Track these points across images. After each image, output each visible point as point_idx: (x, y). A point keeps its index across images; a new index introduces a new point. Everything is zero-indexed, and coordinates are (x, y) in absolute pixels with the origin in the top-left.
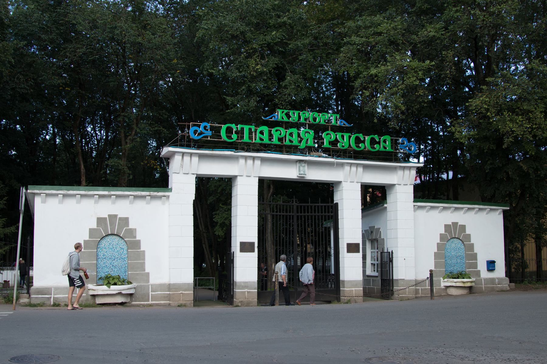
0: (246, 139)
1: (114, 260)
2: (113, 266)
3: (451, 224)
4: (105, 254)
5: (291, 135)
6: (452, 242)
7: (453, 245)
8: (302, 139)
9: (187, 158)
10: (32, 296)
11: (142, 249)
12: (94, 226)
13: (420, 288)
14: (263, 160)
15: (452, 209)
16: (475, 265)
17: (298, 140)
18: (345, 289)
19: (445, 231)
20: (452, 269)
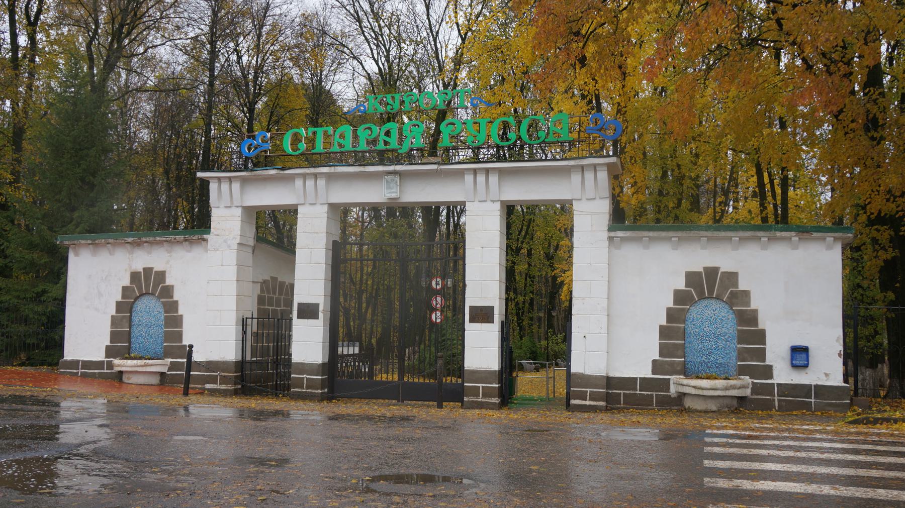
0: (319, 147)
1: (150, 327)
2: (148, 335)
4: (141, 319)
5: (388, 133)
6: (707, 306)
7: (708, 312)
9: (310, 183)
12: (681, 285)
13: (654, 394)
14: (501, 171)
16: (761, 354)
17: (499, 134)
19: (131, 283)
20: (703, 359)
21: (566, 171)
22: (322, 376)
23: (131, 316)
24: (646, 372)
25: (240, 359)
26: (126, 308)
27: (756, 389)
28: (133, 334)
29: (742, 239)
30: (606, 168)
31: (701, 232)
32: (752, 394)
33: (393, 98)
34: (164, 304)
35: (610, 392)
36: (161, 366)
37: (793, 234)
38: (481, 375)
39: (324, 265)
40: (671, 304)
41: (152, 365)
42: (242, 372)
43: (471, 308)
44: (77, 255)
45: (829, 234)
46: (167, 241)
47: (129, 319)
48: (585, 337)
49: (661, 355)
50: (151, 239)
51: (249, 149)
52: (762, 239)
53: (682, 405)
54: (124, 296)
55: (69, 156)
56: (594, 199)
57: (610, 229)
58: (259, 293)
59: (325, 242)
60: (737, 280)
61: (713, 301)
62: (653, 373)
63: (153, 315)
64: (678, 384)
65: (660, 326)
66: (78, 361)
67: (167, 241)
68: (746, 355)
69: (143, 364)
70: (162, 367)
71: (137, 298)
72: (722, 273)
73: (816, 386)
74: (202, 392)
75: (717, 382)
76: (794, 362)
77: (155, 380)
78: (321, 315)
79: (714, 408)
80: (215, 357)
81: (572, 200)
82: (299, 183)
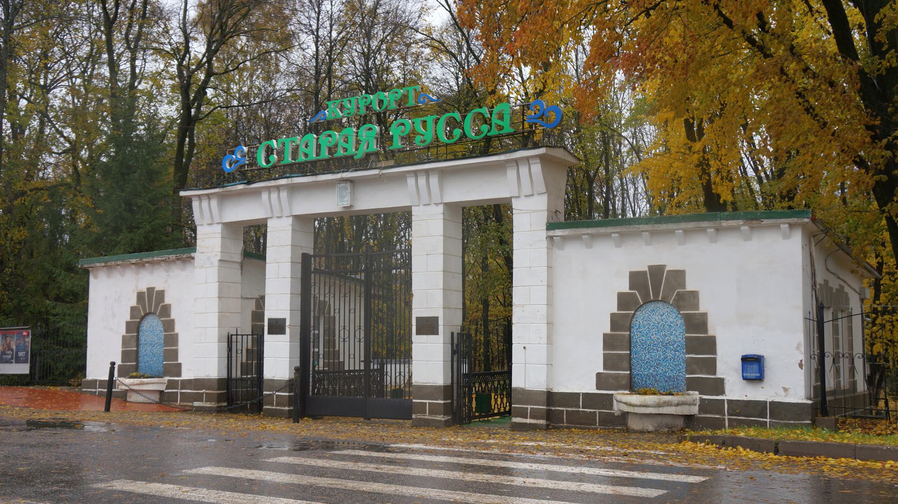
0: (288, 159)
6: (653, 310)
7: (656, 318)
9: (422, 181)
12: (625, 288)
14: (442, 172)
16: (711, 365)
18: (287, 394)
19: (137, 303)
20: (651, 371)
21: (500, 167)
22: (444, 400)
23: (138, 336)
24: (590, 387)
25: (224, 375)
26: (134, 327)
27: (705, 406)
28: (140, 354)
29: (686, 231)
30: (539, 161)
31: (641, 226)
32: (700, 413)
33: (350, 101)
34: (164, 323)
35: (553, 409)
36: (158, 384)
37: (741, 222)
39: (290, 279)
40: (615, 310)
41: (148, 384)
42: (228, 389)
43: (417, 318)
44: (96, 277)
45: (782, 220)
46: (163, 261)
49: (605, 368)
50: (150, 259)
51: (230, 165)
52: (708, 230)
53: (626, 424)
54: (132, 317)
55: (770, 85)
56: (533, 195)
58: (254, 309)
59: (290, 255)
60: (685, 280)
61: (660, 305)
62: (598, 388)
64: (624, 400)
65: (604, 334)
66: (96, 381)
67: (163, 261)
68: (695, 367)
69: (139, 382)
70: (160, 385)
71: (142, 318)
72: (669, 271)
73: (772, 403)
74: (185, 410)
75: (647, 397)
76: (744, 374)
77: (156, 397)
78: (288, 330)
79: (651, 428)
80: (202, 375)
81: (511, 197)
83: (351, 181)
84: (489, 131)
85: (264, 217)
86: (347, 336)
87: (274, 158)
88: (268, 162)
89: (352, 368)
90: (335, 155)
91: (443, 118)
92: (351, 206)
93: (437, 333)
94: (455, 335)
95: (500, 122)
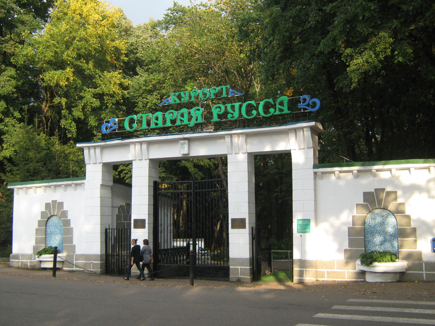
2: (55, 239)
3: (373, 191)
4: (52, 230)
5: (182, 115)
8: (192, 117)
10: (11, 260)
11: (71, 227)
14: (149, 143)
15: (52, 187)
19: (46, 210)
21: (286, 133)
23: (46, 229)
30: (309, 129)
38: (240, 261)
47: (45, 230)
48: (301, 236)
51: (106, 129)
57: (315, 167)
63: (57, 228)
71: (49, 218)
78: (147, 225)
82: (228, 139)
83: (189, 139)
84: (275, 112)
85: (131, 159)
86: (163, 229)
87: (135, 125)
88: (131, 127)
89: (166, 248)
90: (176, 124)
91: (245, 105)
92: (188, 154)
93: (245, 228)
94: (254, 228)
95: (281, 107)
